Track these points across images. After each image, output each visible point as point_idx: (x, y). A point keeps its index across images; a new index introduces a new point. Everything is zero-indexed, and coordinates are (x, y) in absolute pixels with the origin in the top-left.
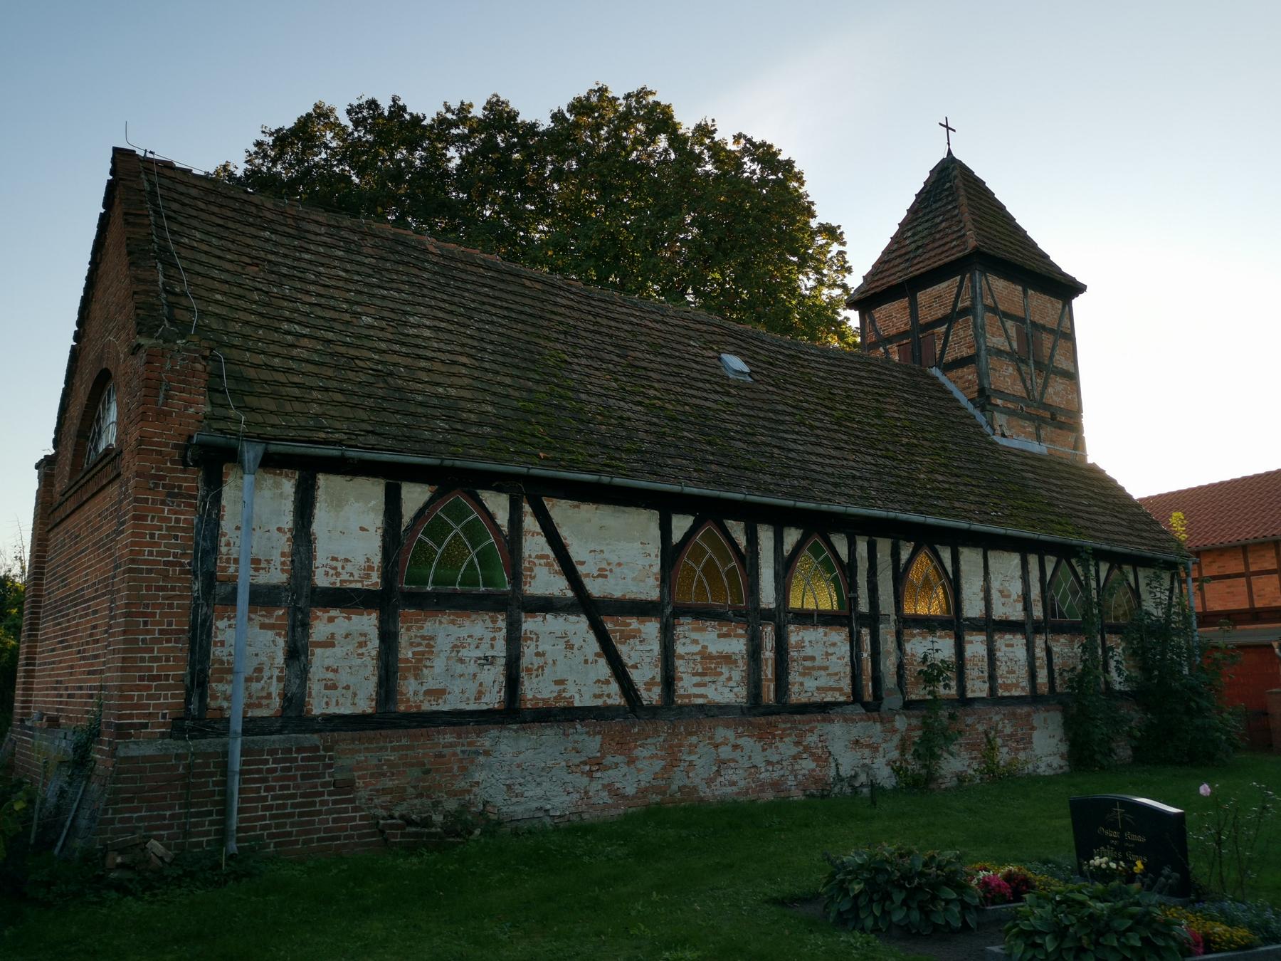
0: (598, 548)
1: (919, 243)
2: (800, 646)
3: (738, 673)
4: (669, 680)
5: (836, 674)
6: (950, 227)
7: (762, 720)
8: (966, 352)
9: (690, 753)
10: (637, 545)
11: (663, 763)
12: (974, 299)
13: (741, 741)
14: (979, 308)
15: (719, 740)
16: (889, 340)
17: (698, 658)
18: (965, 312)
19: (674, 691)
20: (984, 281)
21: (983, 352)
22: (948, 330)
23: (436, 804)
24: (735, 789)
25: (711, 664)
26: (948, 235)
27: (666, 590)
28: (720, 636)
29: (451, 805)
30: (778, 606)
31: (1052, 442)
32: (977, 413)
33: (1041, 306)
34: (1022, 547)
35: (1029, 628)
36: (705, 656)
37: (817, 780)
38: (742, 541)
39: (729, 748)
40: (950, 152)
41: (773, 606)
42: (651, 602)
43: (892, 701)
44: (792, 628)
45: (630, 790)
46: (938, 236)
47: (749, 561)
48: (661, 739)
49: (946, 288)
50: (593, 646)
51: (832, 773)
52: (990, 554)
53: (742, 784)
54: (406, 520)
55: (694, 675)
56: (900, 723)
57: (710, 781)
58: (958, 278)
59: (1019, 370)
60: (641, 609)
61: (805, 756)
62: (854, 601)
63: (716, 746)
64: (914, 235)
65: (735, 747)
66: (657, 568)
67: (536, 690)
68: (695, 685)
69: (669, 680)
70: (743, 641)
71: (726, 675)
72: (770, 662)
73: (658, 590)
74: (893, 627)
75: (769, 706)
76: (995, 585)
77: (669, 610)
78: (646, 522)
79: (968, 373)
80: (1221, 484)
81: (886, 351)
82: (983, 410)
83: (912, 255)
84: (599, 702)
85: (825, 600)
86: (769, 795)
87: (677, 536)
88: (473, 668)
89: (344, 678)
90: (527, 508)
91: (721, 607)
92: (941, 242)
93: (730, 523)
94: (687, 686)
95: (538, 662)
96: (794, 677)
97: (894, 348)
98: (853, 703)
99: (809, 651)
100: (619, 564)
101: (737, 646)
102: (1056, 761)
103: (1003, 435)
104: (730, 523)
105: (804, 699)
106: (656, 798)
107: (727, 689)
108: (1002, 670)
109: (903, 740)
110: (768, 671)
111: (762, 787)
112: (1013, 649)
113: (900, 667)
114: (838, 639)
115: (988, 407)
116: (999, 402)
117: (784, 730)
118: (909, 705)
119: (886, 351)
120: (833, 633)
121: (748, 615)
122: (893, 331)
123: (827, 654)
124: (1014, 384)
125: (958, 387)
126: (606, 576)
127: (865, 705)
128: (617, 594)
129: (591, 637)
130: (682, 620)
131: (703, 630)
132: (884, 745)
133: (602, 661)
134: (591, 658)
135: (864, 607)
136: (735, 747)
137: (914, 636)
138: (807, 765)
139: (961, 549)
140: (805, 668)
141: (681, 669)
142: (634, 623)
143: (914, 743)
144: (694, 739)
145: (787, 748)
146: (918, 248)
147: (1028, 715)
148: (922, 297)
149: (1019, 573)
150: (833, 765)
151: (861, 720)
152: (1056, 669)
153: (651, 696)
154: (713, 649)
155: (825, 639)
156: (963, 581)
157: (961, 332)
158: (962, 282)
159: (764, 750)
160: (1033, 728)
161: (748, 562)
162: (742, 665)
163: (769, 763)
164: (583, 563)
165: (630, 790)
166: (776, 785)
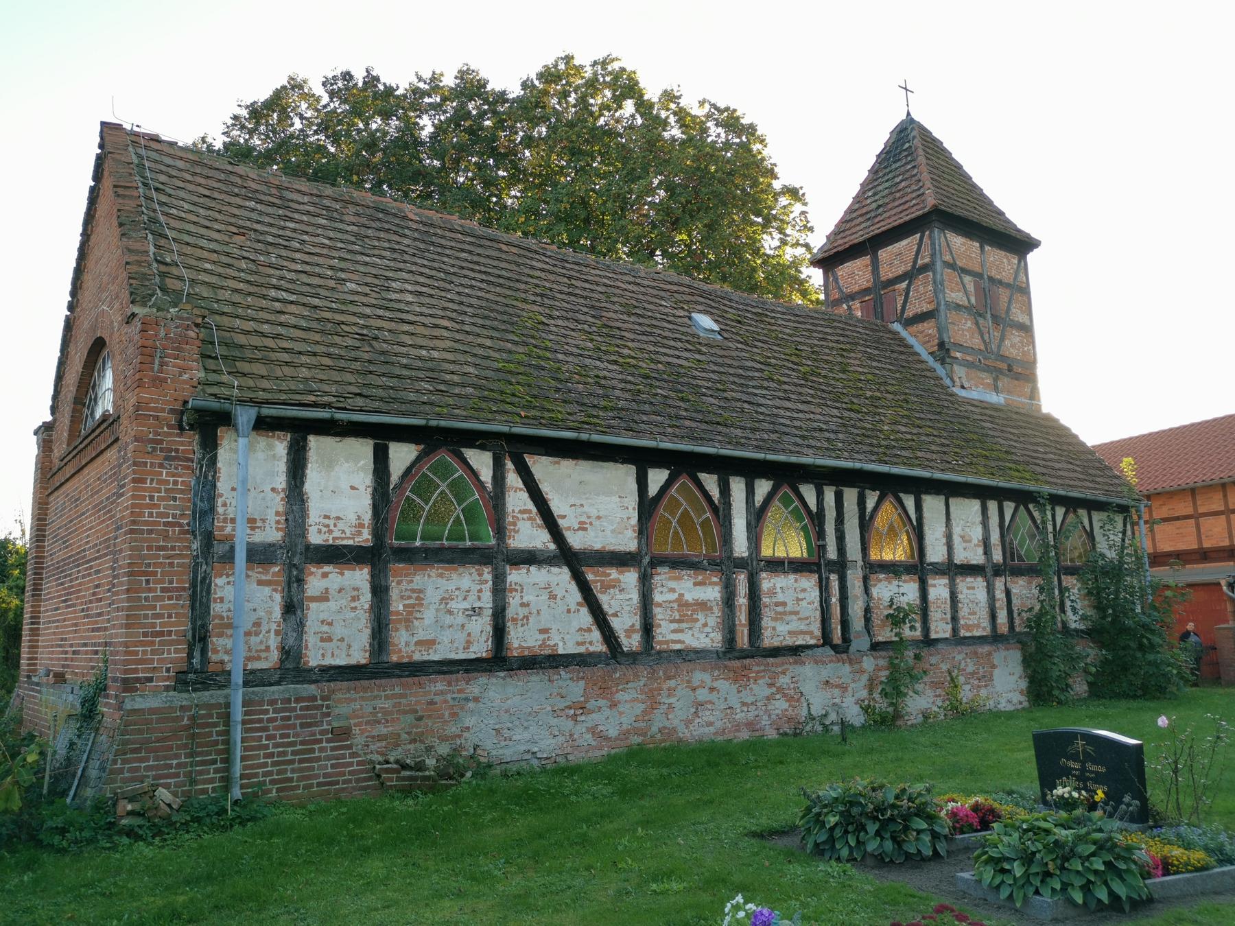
0: (578, 502)
1: (880, 203)
2: (772, 592)
3: (713, 619)
4: (648, 629)
5: (807, 618)
6: (909, 186)
7: (737, 663)
8: (926, 307)
9: (669, 696)
10: (616, 499)
11: (644, 706)
12: (933, 255)
13: (717, 684)
14: (939, 265)
15: (696, 683)
16: (852, 297)
17: (675, 606)
18: (925, 268)
19: (653, 637)
20: (943, 239)
21: (942, 307)
22: (909, 285)
23: (429, 749)
24: (712, 729)
25: (687, 611)
26: (907, 194)
27: (644, 541)
28: (695, 584)
29: (444, 749)
30: (751, 554)
31: (1009, 392)
32: (937, 366)
33: (998, 261)
34: (982, 493)
35: (989, 571)
36: (682, 603)
37: (789, 720)
38: (715, 493)
39: (706, 691)
40: (908, 114)
41: (745, 555)
42: (629, 553)
43: (860, 643)
44: (764, 575)
45: (613, 733)
46: (898, 195)
47: (722, 513)
48: (642, 683)
49: (906, 245)
50: (575, 595)
51: (804, 712)
52: (951, 501)
53: (719, 724)
54: (395, 477)
55: (671, 622)
56: (868, 663)
57: (688, 723)
58: (918, 235)
59: (977, 324)
60: (620, 560)
61: (778, 696)
62: (822, 548)
63: (694, 689)
64: (875, 194)
65: (712, 689)
66: (634, 520)
67: (521, 639)
68: (674, 631)
69: (648, 629)
70: (717, 588)
71: (702, 621)
72: (744, 608)
73: (636, 541)
74: (860, 574)
75: (742, 650)
76: (957, 531)
77: (646, 560)
78: (625, 475)
79: (929, 327)
80: (1215, 420)
81: (849, 308)
82: (943, 362)
83: (873, 214)
84: (582, 650)
85: (795, 547)
86: (745, 735)
87: (653, 490)
88: (461, 619)
89: (338, 631)
90: (509, 465)
91: (697, 556)
92: (901, 201)
93: (703, 476)
94: (665, 633)
95: (522, 612)
96: (766, 622)
97: (856, 304)
98: (823, 645)
99: (780, 597)
100: (599, 518)
101: (713, 593)
102: (1017, 697)
103: (962, 387)
104: (703, 476)
105: (776, 643)
106: (636, 740)
107: (704, 635)
108: (963, 612)
109: (871, 680)
110: (742, 617)
111: (738, 727)
112: (973, 591)
113: (867, 610)
114: (808, 584)
115: (948, 360)
116: (958, 355)
117: (758, 672)
118: (875, 647)
119: (849, 308)
120: (803, 580)
121: (723, 564)
122: (856, 288)
123: (798, 599)
124: (972, 337)
125: (919, 341)
126: (585, 529)
127: (835, 648)
128: (597, 546)
129: (573, 587)
130: (659, 569)
131: (679, 578)
132: (853, 685)
133: (584, 610)
134: (573, 607)
135: (832, 554)
136: (712, 689)
137: (880, 581)
138: (781, 705)
139: (923, 497)
140: (777, 613)
141: (659, 617)
142: (613, 573)
143: (882, 682)
144: (672, 683)
145: (760, 689)
146: (879, 206)
147: (990, 654)
148: (883, 254)
149: (979, 518)
150: (805, 704)
151: (831, 661)
152: (1015, 609)
153: (631, 642)
154: (689, 597)
155: (796, 585)
156: (926, 528)
157: (921, 288)
158: (921, 239)
159: (739, 692)
160: (994, 666)
161: (721, 513)
162: (717, 612)
163: (744, 704)
164: (564, 517)
165: (613, 733)
166: (750, 725)
